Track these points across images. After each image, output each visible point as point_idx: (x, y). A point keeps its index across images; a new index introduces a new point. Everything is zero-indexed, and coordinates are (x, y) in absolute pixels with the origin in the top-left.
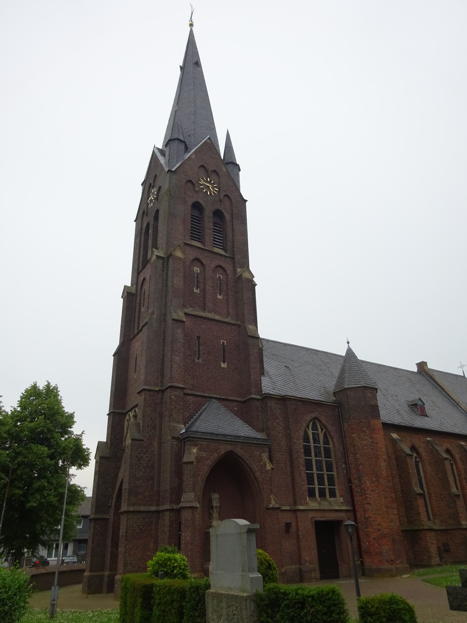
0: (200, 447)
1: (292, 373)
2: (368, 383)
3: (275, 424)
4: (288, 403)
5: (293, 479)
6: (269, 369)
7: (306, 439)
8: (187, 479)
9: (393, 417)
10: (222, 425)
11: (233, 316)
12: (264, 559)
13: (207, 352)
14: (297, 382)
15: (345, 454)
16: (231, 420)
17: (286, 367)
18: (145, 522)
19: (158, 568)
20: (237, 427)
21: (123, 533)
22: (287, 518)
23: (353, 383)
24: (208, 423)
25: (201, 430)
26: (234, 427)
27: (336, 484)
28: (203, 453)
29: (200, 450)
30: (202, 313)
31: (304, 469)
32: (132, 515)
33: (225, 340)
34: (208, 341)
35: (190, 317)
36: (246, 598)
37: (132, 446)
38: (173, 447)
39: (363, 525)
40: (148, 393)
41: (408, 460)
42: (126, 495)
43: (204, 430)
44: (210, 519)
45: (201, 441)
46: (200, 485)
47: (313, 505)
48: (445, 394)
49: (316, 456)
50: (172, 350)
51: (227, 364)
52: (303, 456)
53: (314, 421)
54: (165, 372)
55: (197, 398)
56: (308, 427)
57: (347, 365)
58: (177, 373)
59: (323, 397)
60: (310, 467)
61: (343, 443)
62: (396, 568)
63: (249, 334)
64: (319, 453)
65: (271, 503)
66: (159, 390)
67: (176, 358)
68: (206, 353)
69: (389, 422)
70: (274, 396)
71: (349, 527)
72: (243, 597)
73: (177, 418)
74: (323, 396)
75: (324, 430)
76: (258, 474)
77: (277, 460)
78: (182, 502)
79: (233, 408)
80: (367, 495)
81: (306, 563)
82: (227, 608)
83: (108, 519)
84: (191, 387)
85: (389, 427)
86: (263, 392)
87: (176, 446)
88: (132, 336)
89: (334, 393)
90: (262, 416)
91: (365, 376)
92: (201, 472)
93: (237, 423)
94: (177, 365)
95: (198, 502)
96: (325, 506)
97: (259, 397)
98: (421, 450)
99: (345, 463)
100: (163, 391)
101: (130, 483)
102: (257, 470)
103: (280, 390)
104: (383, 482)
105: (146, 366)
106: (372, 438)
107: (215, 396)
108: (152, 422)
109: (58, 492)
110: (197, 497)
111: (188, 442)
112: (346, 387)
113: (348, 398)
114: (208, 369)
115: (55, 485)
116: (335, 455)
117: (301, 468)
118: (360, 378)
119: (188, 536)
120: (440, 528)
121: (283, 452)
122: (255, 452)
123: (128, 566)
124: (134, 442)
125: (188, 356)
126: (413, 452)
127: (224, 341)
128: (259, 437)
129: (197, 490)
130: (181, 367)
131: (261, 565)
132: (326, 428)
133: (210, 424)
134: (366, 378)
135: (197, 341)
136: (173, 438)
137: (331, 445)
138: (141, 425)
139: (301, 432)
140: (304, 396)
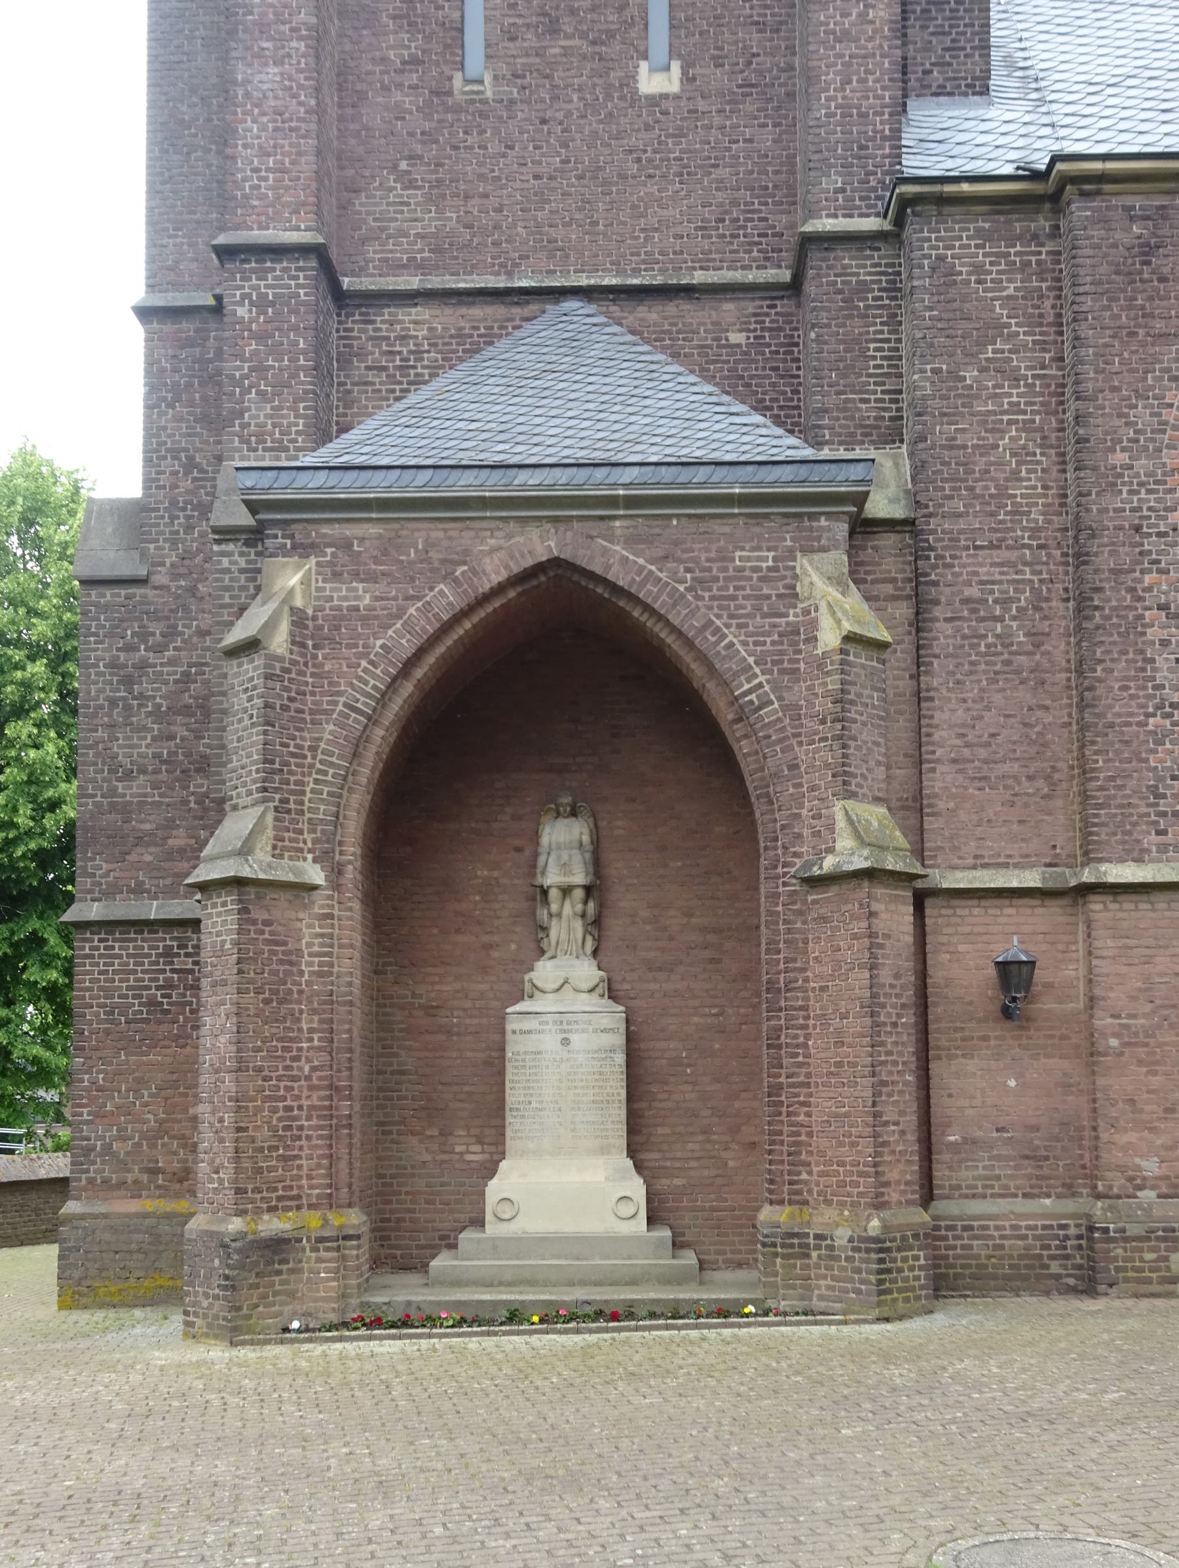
0: (333, 555)
3: (970, 375)
18: (173, 971)
28: (356, 589)
29: (337, 576)
32: (100, 940)
38: (227, 582)
45: (339, 521)
46: (332, 765)
55: (463, 311)
58: (268, 170)
65: (831, 850)
67: (263, 77)
68: (528, 26)
70: (965, 187)
73: (274, 426)
77: (967, 601)
79: (718, 339)
81: (1140, 1188)
84: (422, 251)
87: (243, 577)
90: (888, 341)
92: (339, 694)
94: (265, 119)
95: (315, 861)
102: (751, 660)
108: (195, 480)
110: (314, 831)
114: (544, 121)
121: (1024, 546)
122: (738, 554)
123: (94, 1163)
124: (93, 593)
125: (402, 71)
129: (309, 795)
130: (291, 129)
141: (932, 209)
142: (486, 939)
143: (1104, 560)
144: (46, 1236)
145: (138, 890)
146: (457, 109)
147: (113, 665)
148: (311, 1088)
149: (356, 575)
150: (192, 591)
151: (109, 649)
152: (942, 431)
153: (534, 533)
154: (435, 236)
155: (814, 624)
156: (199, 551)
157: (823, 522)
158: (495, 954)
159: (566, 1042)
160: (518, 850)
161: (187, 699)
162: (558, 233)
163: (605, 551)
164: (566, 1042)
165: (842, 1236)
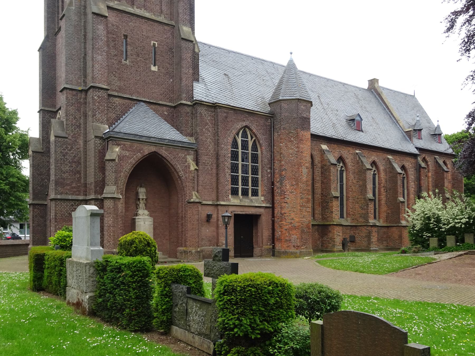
1: (230, 82)
2: (303, 96)
3: (204, 130)
4: (219, 110)
5: (218, 179)
6: (205, 75)
7: (235, 144)
8: (109, 174)
9: (326, 130)
10: (148, 127)
11: (167, 14)
12: (143, 239)
13: (135, 53)
14: (234, 91)
15: (272, 160)
16: (157, 123)
17: (225, 74)
19: (58, 242)
20: (163, 130)
21: (53, 216)
22: (209, 210)
23: (288, 95)
24: (133, 125)
25: (125, 131)
26: (160, 131)
27: (260, 185)
29: (123, 150)
30: (130, 9)
31: (230, 171)
33: (157, 41)
34: (137, 41)
35: (116, 12)
36: (86, 265)
37: (55, 142)
39: (278, 219)
40: (71, 92)
41: (332, 168)
42: (54, 185)
43: (127, 131)
44: (137, 208)
47: (234, 201)
48: (388, 111)
49: (243, 161)
50: (93, 48)
51: (158, 67)
52: (229, 160)
53: (244, 129)
54: (88, 71)
55: (124, 100)
56: (238, 134)
57: (286, 76)
59: (258, 107)
60: (235, 170)
61: (271, 151)
62: (300, 252)
63: (183, 37)
64: (246, 158)
65: (192, 198)
66: (82, 90)
69: (321, 134)
70: (204, 103)
71: (226, 217)
72: (84, 263)
74: (259, 106)
75: (254, 138)
76: (181, 173)
77: (203, 163)
78: (105, 193)
80: (285, 196)
82: (76, 271)
83: (46, 205)
85: (316, 138)
86: (194, 99)
88: (57, 30)
89: (269, 104)
91: (301, 89)
93: (164, 127)
96: (246, 202)
97: (189, 103)
98: (347, 161)
99: (271, 168)
100: (86, 91)
101: (55, 175)
103: (213, 98)
104: (302, 186)
105: (66, 64)
106: (298, 147)
107: (144, 100)
109: (9, 181)
111: (110, 142)
112: (281, 98)
113: (281, 109)
114: (137, 71)
115: (5, 175)
116: (262, 161)
117: (226, 171)
118: (296, 90)
119: (110, 220)
120: (350, 224)
126: (372, 167)
127: (155, 42)
128: (185, 141)
131: (139, 243)
132: (256, 136)
133: (135, 126)
134: (302, 91)
135: (125, 40)
136: (96, 137)
137: (259, 152)
138: (65, 123)
139: (229, 138)
140: (239, 105)
141: (200, 105)
142: (128, 206)
143: (221, 160)
144: (26, 254)
145: (67, 194)
146: (123, 65)
147: (61, 152)
148: (120, 230)
149: (126, 150)
150: (76, 141)
151: (60, 149)
152: (201, 137)
153: (152, 147)
154: (119, 86)
155: (190, 166)
156: (77, 134)
157: (190, 151)
158: (130, 208)
159: (145, 223)
160: (133, 192)
161: (75, 160)
162: (139, 90)
163: (162, 151)
164: (145, 223)
165: (194, 251)
